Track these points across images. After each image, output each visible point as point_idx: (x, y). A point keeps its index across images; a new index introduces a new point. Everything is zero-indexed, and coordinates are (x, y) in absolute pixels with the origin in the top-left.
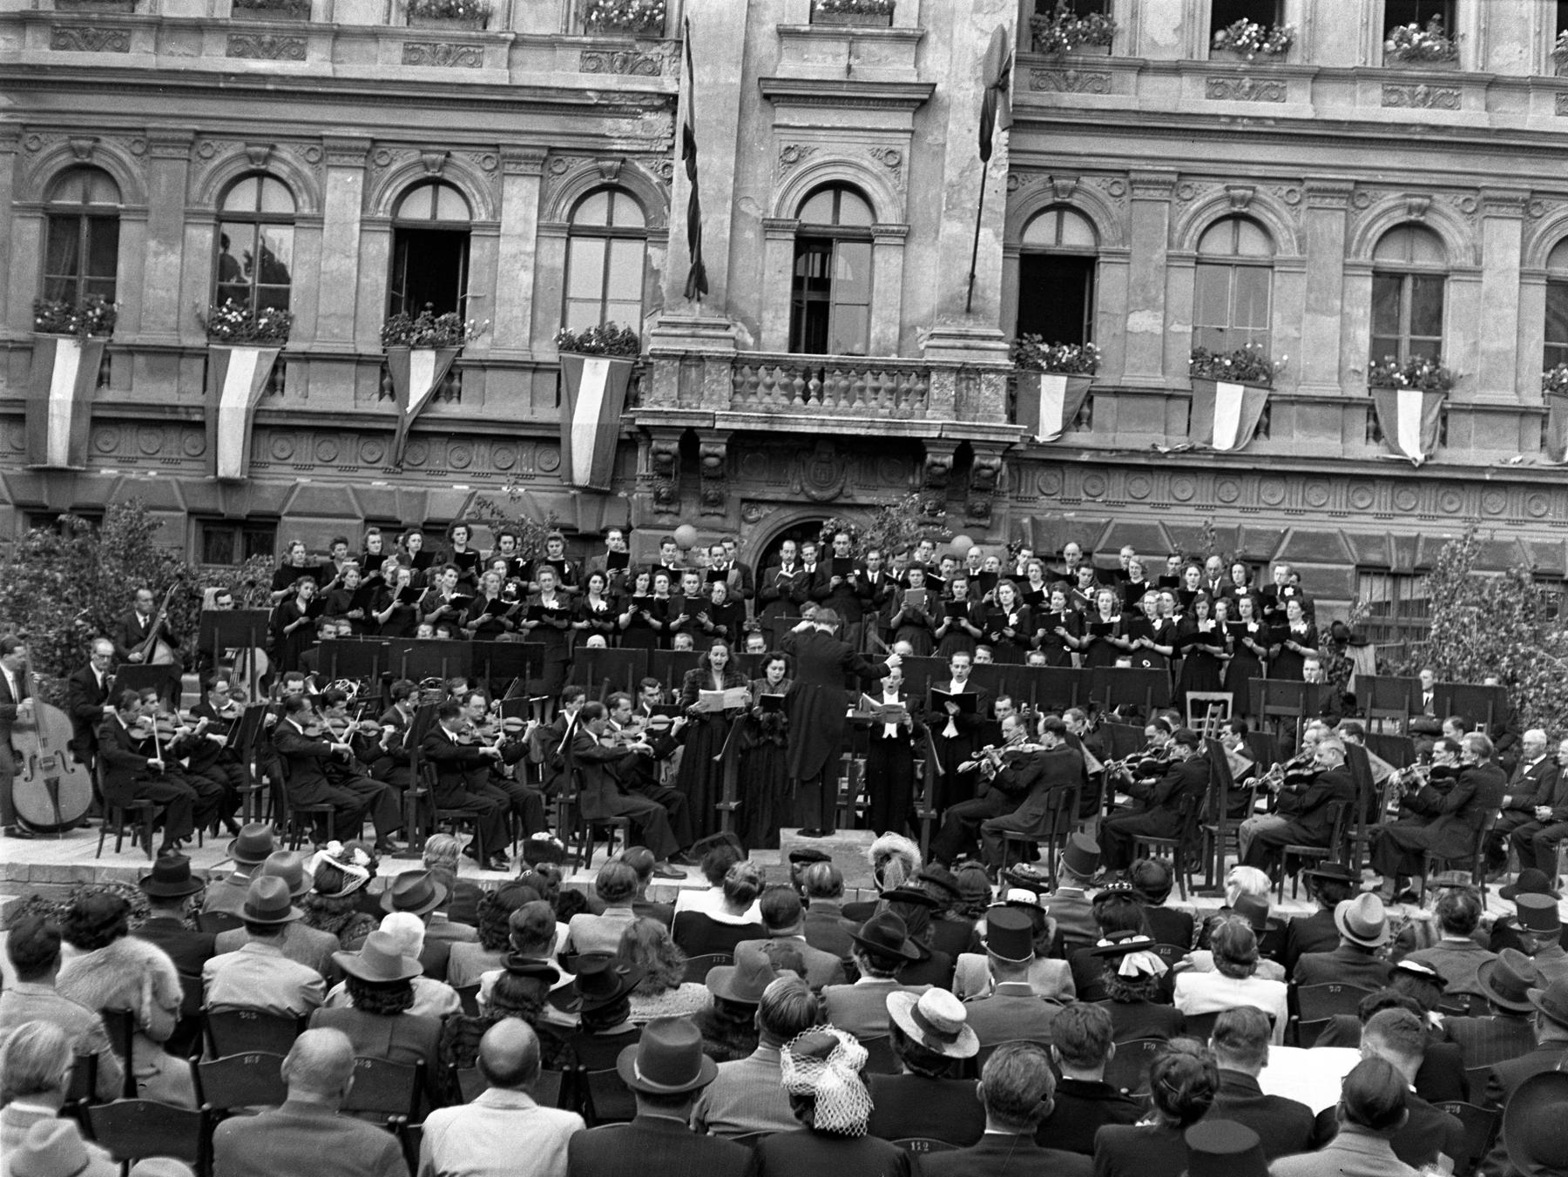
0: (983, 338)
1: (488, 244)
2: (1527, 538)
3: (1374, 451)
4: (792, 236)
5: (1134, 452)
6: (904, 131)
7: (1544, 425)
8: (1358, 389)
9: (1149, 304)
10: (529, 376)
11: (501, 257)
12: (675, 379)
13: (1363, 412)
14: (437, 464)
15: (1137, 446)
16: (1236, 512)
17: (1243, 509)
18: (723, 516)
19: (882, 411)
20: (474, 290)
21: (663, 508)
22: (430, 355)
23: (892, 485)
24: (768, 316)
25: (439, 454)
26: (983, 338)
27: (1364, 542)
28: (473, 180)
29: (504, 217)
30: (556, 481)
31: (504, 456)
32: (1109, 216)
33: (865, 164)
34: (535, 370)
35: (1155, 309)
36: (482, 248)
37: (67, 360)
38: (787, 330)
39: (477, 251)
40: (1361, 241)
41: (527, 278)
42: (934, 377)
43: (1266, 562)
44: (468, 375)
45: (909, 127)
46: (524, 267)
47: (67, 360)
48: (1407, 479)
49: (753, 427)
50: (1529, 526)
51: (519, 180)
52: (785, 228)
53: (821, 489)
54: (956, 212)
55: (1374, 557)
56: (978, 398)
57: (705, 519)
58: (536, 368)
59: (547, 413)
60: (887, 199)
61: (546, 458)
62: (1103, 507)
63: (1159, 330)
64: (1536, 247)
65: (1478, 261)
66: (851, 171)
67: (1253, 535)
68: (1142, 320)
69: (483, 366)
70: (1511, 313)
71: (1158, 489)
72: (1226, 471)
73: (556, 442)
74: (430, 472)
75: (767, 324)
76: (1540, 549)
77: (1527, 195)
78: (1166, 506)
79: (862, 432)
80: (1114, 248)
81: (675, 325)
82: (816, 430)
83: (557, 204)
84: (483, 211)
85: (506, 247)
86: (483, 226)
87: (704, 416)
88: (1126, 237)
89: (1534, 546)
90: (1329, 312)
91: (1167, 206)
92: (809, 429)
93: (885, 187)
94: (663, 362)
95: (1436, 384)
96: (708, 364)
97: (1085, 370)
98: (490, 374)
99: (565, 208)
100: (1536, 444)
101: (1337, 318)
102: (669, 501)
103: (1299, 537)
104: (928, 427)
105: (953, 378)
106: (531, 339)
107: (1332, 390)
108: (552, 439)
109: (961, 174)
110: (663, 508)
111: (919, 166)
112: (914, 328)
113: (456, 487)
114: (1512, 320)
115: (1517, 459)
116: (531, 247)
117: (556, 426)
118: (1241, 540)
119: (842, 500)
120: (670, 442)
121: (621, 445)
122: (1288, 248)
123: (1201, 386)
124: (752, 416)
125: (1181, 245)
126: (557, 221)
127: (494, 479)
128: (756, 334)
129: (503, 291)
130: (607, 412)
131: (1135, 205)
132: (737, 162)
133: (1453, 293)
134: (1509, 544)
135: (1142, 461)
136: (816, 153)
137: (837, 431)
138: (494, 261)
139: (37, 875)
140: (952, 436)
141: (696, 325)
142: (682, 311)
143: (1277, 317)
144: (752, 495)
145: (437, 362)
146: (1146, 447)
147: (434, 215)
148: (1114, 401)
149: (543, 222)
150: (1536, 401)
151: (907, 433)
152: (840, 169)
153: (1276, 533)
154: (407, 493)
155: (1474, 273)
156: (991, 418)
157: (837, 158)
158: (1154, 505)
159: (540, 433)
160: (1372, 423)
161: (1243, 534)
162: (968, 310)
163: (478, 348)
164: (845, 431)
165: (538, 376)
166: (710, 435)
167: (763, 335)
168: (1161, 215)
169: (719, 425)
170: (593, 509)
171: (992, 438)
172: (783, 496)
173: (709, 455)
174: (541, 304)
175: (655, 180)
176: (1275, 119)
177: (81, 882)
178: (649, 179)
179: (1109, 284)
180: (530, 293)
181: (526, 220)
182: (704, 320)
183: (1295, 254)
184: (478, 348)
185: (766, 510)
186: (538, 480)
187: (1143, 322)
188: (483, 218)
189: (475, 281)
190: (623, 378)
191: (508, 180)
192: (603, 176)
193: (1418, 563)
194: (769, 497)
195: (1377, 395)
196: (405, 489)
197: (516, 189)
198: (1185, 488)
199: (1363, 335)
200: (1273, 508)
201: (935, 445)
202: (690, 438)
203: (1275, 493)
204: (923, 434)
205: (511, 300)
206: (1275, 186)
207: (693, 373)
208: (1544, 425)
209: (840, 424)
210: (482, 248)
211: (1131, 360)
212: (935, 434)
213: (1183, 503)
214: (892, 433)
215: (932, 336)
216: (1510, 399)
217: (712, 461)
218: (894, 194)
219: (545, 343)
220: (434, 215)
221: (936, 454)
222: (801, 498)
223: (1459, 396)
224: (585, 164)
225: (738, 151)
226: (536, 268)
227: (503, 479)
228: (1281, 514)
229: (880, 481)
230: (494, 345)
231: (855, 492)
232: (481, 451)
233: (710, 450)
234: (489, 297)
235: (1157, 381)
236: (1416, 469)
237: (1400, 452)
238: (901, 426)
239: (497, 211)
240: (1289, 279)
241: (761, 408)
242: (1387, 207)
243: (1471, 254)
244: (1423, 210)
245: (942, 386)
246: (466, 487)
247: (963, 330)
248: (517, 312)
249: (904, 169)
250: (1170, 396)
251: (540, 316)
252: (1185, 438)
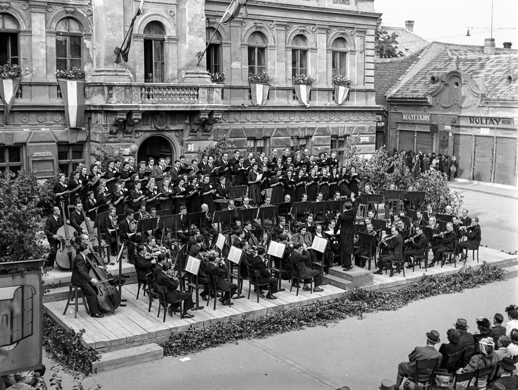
0: (202, 74)
1: (27, 39)
2: (331, 126)
3: (295, 103)
4: (143, 40)
5: (238, 107)
6: (175, 4)
7: (334, 93)
8: (290, 85)
9: (237, 59)
10: (48, 87)
11: (33, 43)
12: (123, 94)
13: (292, 91)
14: (17, 122)
15: (238, 105)
16: (262, 123)
17: (264, 122)
18: (131, 137)
19: (186, 101)
20: (23, 56)
21: (112, 136)
22: (10, 81)
23: (180, 123)
24: (138, 67)
25: (18, 118)
26: (202, 74)
27: (293, 129)
28: (20, 14)
29: (33, 28)
30: (61, 125)
31: (41, 118)
32: (224, 31)
33: (164, 15)
34: (49, 86)
35: (239, 61)
36: (25, 40)
37: (72, 88)
38: (144, 72)
39: (22, 41)
40: (289, 40)
41: (43, 51)
42: (200, 90)
43: (269, 137)
44: (24, 88)
45: (176, 3)
46: (42, 47)
47: (72, 88)
48: (304, 111)
49: (151, 109)
50: (331, 122)
51: (37, 14)
52: (141, 37)
53: (160, 126)
54: (192, 32)
55: (296, 133)
56: (212, 96)
57: (124, 139)
58: (50, 85)
59: (57, 102)
60: (171, 27)
61: (58, 118)
62: (228, 124)
63: (240, 68)
64: (330, 41)
65: (316, 46)
66: (159, 17)
67: (267, 130)
68: (235, 65)
69: (30, 85)
70: (325, 61)
71: (242, 117)
72: (261, 111)
73: (64, 111)
74: (14, 125)
75: (137, 70)
76: (333, 129)
77: (328, 27)
78: (244, 122)
79: (184, 109)
80: (226, 42)
81: (109, 71)
82: (170, 109)
83: (51, 23)
84: (24, 26)
85: (34, 40)
86: (25, 32)
87: (136, 106)
88: (230, 38)
89: (332, 128)
90: (282, 61)
91: (240, 28)
92: (168, 109)
93: (170, 23)
94: (119, 88)
95: (309, 83)
96: (133, 88)
97: (221, 81)
98: (33, 87)
99: (54, 25)
100: (331, 99)
101: (284, 63)
102: (114, 134)
103: (278, 129)
104: (203, 107)
105: (206, 90)
106: (47, 74)
107: (284, 85)
108: (62, 111)
109: (192, 20)
110: (112, 136)
111: (179, 16)
112: (181, 70)
113: (24, 130)
114: (325, 63)
115: (329, 104)
116: (44, 40)
117: (63, 107)
118: (263, 132)
119: (167, 129)
120: (123, 115)
121: (87, 113)
122: (271, 43)
123: (252, 85)
124: (149, 105)
125: (244, 41)
126: (52, 30)
127: (38, 126)
128: (134, 73)
129: (35, 56)
130: (79, 101)
131: (232, 28)
132: (124, 14)
133: (309, 54)
134: (326, 128)
135: (240, 109)
136: (148, 11)
137: (176, 109)
138: (30, 45)
139: (158, 334)
140: (209, 109)
141: (116, 71)
142: (111, 66)
143: (269, 63)
144: (139, 129)
145: (13, 83)
146: (241, 105)
147: (4, 27)
148: (229, 90)
149: (47, 30)
150: (331, 87)
151: (196, 109)
152: (156, 17)
153: (272, 129)
154: (8, 134)
155: (315, 50)
156: (218, 103)
157: (155, 13)
158: (241, 122)
159: (56, 109)
160: (61, 34)
161: (264, 130)
162: (198, 65)
163: (27, 78)
164: (179, 109)
165: (51, 87)
166: (136, 113)
167: (136, 74)
168: (238, 31)
169: (140, 109)
170: (74, 135)
171: (220, 109)
172: (149, 129)
173: (136, 119)
174: (48, 61)
175: (85, 15)
176: (268, 3)
177: (173, 333)
178: (83, 15)
179: (225, 53)
180: (45, 57)
181: (41, 30)
182: (118, 69)
183: (273, 44)
184: (27, 78)
185: (141, 133)
186: (54, 126)
187: (236, 65)
188: (25, 28)
189: (23, 52)
190: (82, 88)
191: (33, 14)
192: (67, 13)
193: (306, 134)
194: (144, 129)
195: (296, 86)
196: (6, 132)
197: (36, 18)
198: (249, 116)
199: (290, 68)
200: (271, 121)
201: (204, 112)
202: (129, 114)
203: (271, 116)
204: (202, 109)
205: (38, 60)
206: (266, 23)
207: (128, 91)
208: (334, 93)
209: (178, 107)
210: (25, 40)
211: (233, 77)
212: (205, 109)
213: (248, 121)
214: (193, 109)
215: (187, 74)
216: (326, 87)
217: (137, 121)
218: (173, 26)
219: (51, 75)
220: (4, 27)
221: (203, 115)
222: (155, 129)
223: (314, 86)
224: (60, 9)
225: (124, 10)
226: (47, 48)
227: (41, 126)
228: (273, 123)
229: (177, 122)
230: (33, 76)
231: (169, 126)
232: (33, 116)
233: (136, 117)
234: (29, 58)
235: (241, 84)
236: (307, 108)
237: (303, 104)
238: (195, 107)
239: (30, 26)
240: (272, 51)
241: (150, 102)
242: (294, 30)
243: (314, 44)
244: (303, 31)
245: (204, 93)
246: (28, 130)
247: (197, 71)
248: (41, 64)
249: (175, 17)
250: (243, 88)
251: (49, 65)
252: (250, 101)
